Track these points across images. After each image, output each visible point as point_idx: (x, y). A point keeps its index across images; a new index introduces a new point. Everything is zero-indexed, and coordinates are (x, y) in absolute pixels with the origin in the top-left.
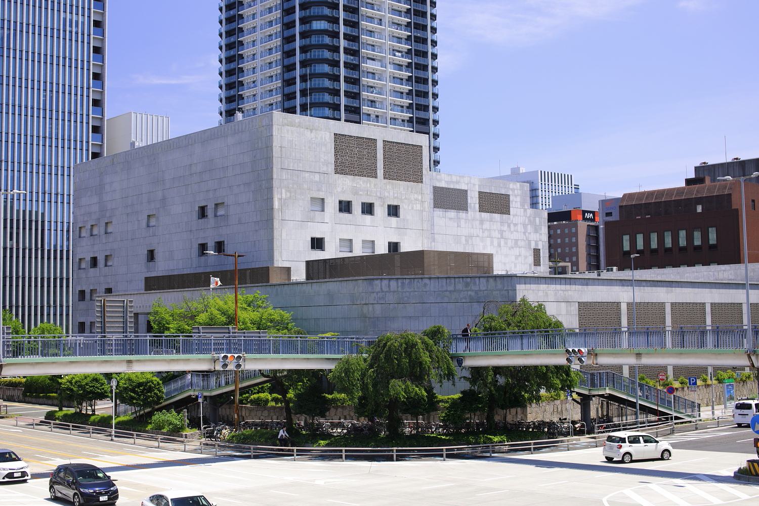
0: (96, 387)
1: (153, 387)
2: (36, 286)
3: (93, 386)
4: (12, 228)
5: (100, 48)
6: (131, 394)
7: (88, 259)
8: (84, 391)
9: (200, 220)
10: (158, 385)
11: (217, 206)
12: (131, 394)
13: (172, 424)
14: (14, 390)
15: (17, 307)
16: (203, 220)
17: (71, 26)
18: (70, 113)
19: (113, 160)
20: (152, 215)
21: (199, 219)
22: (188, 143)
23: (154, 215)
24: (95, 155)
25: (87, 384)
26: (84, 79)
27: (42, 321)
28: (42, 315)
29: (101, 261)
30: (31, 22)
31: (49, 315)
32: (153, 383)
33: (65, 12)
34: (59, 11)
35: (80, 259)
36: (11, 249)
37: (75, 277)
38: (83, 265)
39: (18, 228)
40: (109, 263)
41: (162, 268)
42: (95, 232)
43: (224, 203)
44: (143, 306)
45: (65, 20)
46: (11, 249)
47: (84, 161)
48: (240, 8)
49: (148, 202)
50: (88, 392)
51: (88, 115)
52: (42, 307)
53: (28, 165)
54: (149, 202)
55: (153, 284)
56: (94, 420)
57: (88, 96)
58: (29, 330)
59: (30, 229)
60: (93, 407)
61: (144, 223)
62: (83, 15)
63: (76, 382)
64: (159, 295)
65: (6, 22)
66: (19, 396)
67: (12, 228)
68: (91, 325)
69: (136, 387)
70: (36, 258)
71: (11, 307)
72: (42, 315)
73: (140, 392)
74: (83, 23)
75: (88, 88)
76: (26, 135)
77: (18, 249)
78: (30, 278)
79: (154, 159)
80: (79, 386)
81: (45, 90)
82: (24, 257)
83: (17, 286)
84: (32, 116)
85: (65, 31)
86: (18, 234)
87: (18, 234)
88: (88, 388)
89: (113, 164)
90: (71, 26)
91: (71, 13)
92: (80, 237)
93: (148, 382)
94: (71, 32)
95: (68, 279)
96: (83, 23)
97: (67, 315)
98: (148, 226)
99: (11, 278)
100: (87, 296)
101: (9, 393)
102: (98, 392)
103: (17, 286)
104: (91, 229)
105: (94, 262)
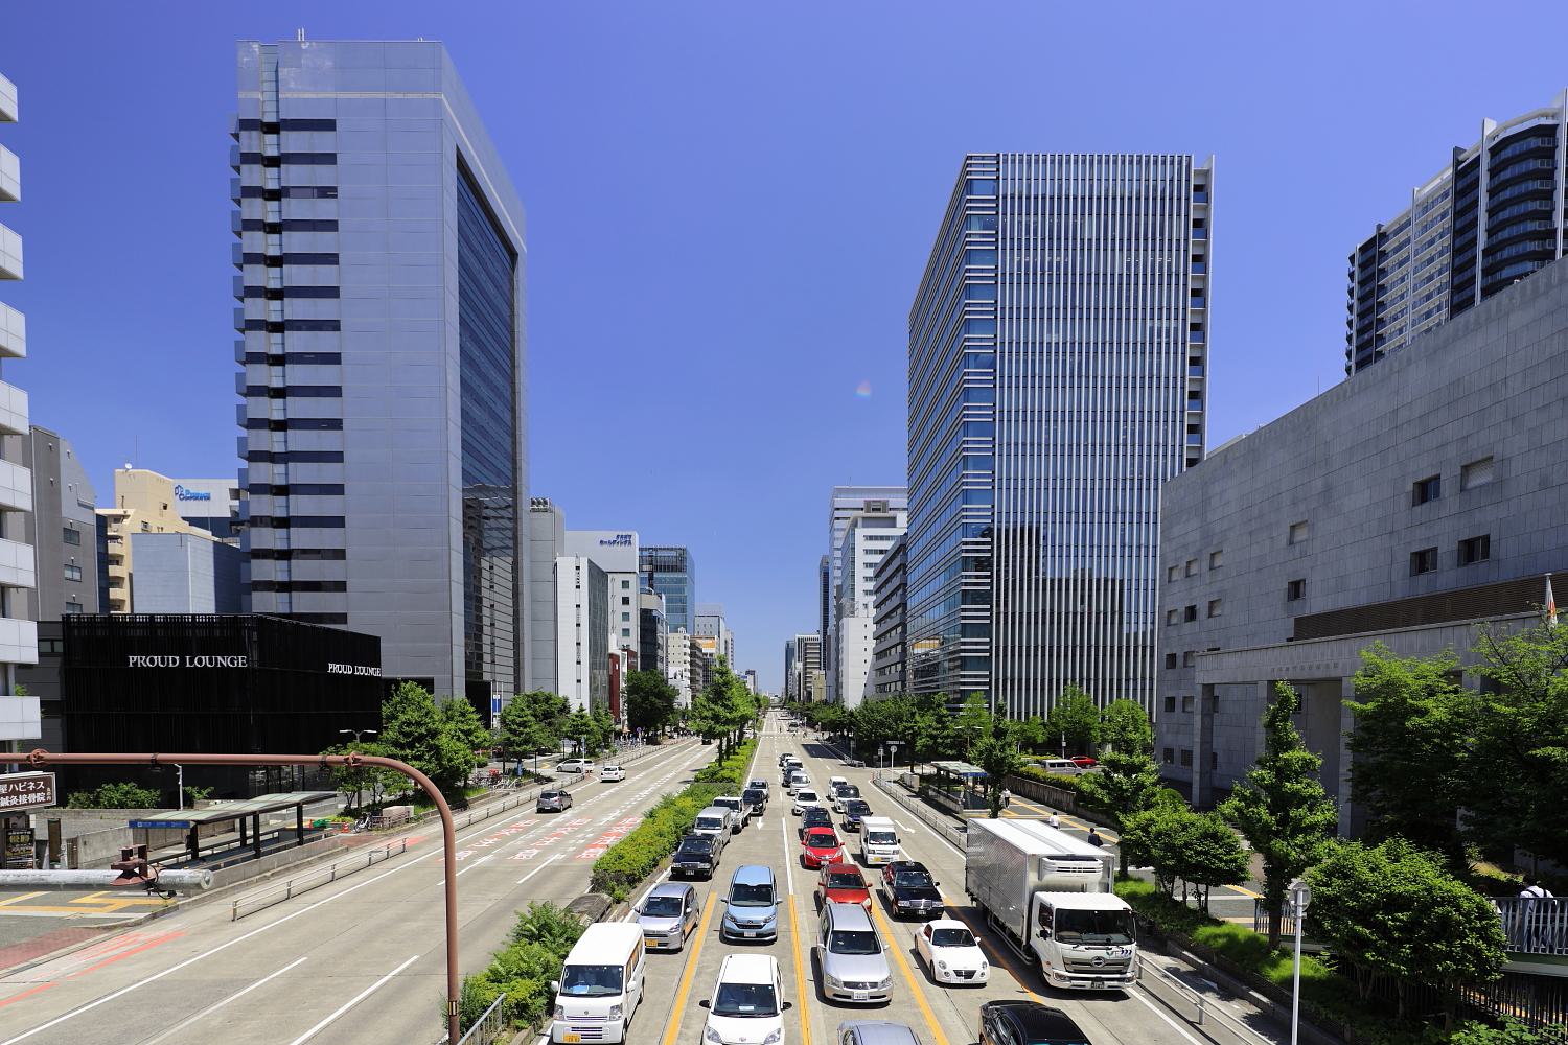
0: (1214, 856)
1: (1459, 923)
2: (1112, 656)
3: (1206, 853)
4: (1083, 589)
5: (1199, 358)
6: (1359, 928)
7: (1182, 610)
8: (1181, 860)
9: (1418, 509)
10: (1480, 918)
11: (1467, 471)
12: (1359, 928)
13: (1346, 876)
14: (1062, 793)
15: (1089, 680)
16: (1426, 505)
17: (1160, 336)
18: (1157, 445)
19: (1226, 456)
20: (1300, 524)
21: (1414, 505)
22: (1391, 370)
23: (1306, 521)
24: (1192, 462)
25: (1187, 845)
26: (1179, 399)
27: (1119, 696)
28: (1119, 689)
29: (1202, 611)
30: (1143, 542)
31: (1127, 689)
32: (1458, 908)
33: (1152, 318)
34: (1144, 319)
35: (1170, 612)
36: (1082, 614)
37: (1162, 636)
38: (1174, 620)
39: (1090, 589)
40: (1215, 613)
41: (1318, 602)
42: (1194, 569)
43: (1492, 457)
44: (1295, 668)
45: (1152, 329)
46: (1082, 614)
47: (1177, 474)
48: (1379, 343)
49: (1294, 503)
50: (1189, 865)
51: (1182, 445)
52: (1119, 680)
53: (1104, 514)
54: (1294, 503)
55: (1310, 628)
56: (1208, 939)
57: (1183, 388)
58: (1103, 706)
59: (1106, 590)
60: (1203, 898)
61: (1284, 541)
62: (1176, 319)
63: (1159, 834)
64: (1334, 646)
65: (1076, 344)
66: (1069, 804)
67: (1083, 589)
68: (1184, 702)
69: (1376, 906)
70: (1113, 623)
71: (1081, 680)
72: (1119, 689)
73: (1397, 928)
74: (1176, 329)
75: (1182, 412)
76: (1101, 479)
77: (1090, 614)
78: (1105, 647)
79: (1308, 429)
80: (1169, 847)
81: (1125, 421)
82: (1097, 623)
83: (1089, 656)
84: (1109, 455)
85: (1151, 343)
86: (1090, 596)
87: (1090, 596)
88: (1190, 857)
89: (1226, 462)
90: (1160, 336)
91: (1160, 319)
92: (1169, 581)
93: (1435, 903)
94: (1160, 343)
95: (1152, 647)
96: (1176, 329)
97: (1151, 689)
98: (1291, 543)
99: (1082, 647)
100: (1180, 662)
101: (1056, 796)
102: (1218, 869)
103: (1089, 656)
104: (1188, 568)
105: (1191, 613)
